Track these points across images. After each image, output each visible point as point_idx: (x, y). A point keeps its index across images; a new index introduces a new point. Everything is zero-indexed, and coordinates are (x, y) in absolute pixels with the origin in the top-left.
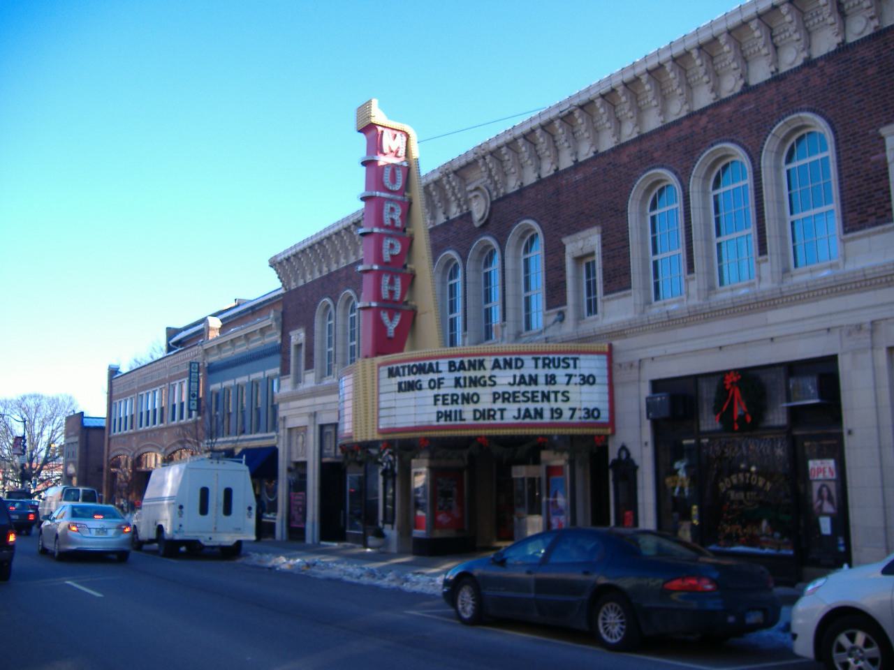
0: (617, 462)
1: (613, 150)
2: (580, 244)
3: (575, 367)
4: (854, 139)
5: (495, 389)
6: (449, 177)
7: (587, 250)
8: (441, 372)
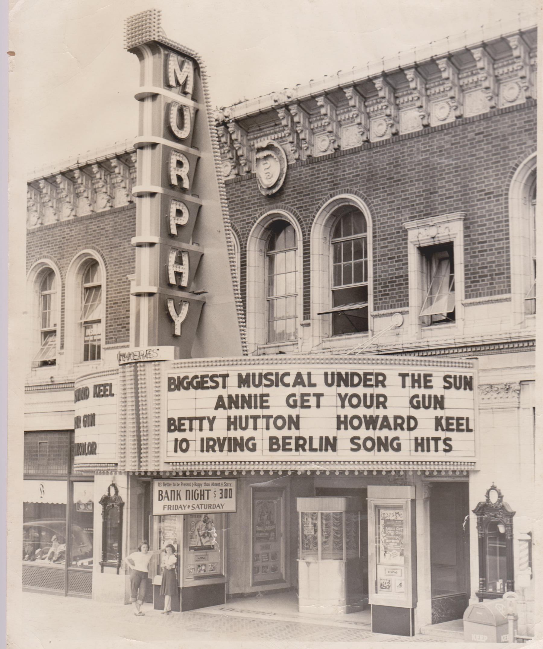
0: (483, 509)
1: (484, 117)
2: (432, 232)
3: (224, 387)
4: (383, 173)
5: (439, 413)
6: (228, 128)
7: (443, 239)
8: (315, 385)
